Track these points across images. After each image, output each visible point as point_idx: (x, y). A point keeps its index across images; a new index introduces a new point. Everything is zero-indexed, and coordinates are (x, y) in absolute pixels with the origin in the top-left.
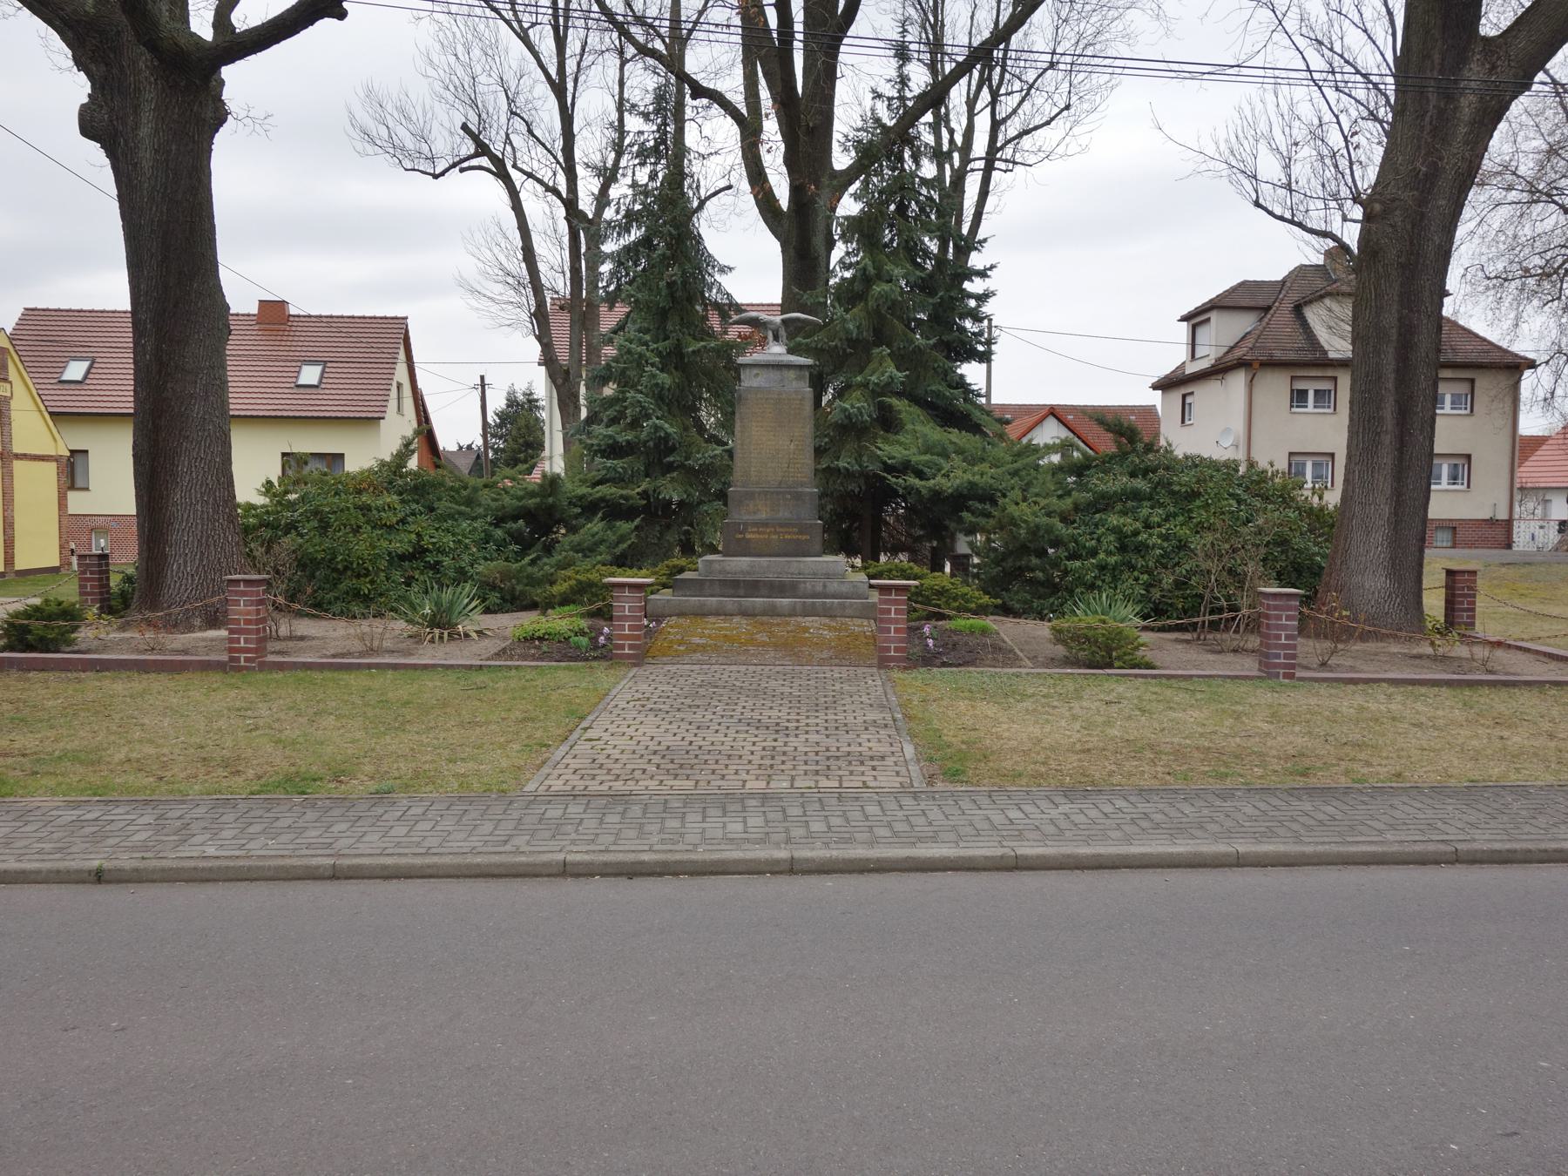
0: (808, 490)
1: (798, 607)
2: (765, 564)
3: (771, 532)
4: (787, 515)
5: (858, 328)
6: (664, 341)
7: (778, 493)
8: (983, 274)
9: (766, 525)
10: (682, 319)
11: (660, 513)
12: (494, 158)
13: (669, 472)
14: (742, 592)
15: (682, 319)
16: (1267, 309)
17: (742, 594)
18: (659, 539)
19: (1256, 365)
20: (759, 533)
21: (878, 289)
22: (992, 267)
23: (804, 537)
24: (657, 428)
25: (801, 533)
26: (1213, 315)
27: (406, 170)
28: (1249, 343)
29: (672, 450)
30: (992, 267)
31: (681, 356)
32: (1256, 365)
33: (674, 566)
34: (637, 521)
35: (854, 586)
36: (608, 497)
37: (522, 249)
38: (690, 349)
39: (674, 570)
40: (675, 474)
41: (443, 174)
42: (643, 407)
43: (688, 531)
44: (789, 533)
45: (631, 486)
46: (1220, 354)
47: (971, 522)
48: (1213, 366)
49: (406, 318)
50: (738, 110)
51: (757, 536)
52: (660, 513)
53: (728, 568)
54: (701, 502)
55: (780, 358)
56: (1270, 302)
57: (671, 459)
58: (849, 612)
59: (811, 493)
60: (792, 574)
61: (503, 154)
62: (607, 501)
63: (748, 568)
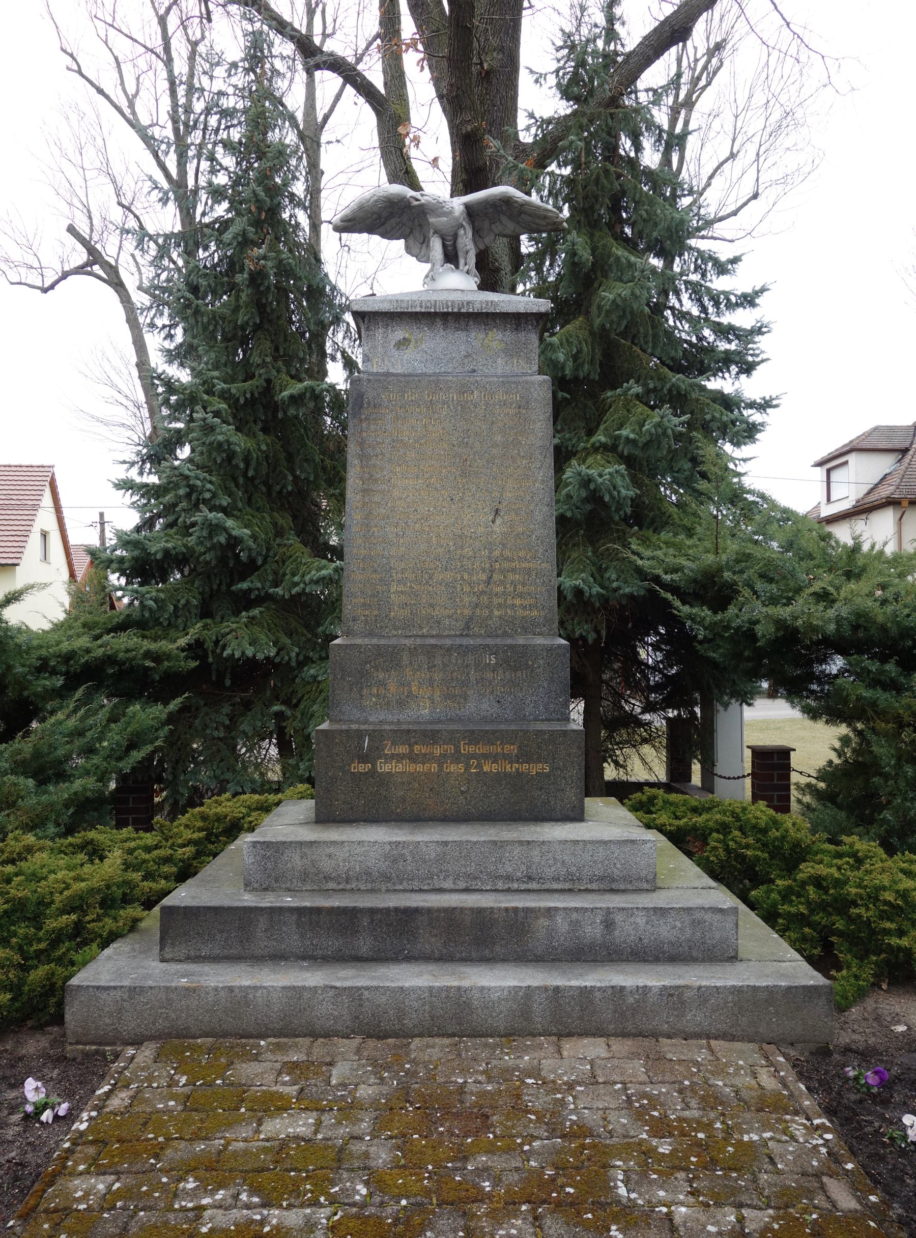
0: (540, 641)
1: (538, 1006)
2: (432, 853)
3: (444, 756)
4: (487, 707)
5: (575, 358)
6: (244, 381)
7: (464, 651)
8: (748, 300)
9: (431, 737)
10: (277, 349)
11: (228, 682)
12: (105, 265)
13: (247, 609)
14: (364, 944)
15: (277, 349)
16: (904, 451)
17: (364, 950)
18: (228, 729)
19: (905, 503)
20: (412, 758)
21: (611, 297)
22: (763, 290)
23: (534, 769)
24: (214, 528)
25: (525, 756)
26: (852, 458)
27: (12, 283)
28: (895, 480)
29: (250, 568)
30: (763, 290)
31: (272, 407)
32: (905, 503)
33: (219, 818)
34: (175, 705)
35: (696, 923)
36: (121, 655)
37: (137, 365)
38: (286, 393)
39: (218, 828)
40: (256, 612)
41: (52, 287)
42: (192, 488)
43: (282, 713)
44: (495, 759)
45: (172, 633)
46: (861, 495)
47: (859, 698)
48: (854, 507)
49: (52, 467)
50: (371, 85)
51: (411, 768)
52: (228, 682)
53: (326, 865)
54: (301, 664)
55: (470, 297)
56: (907, 445)
57: (245, 585)
58: (694, 1018)
59: (550, 649)
60: (509, 878)
61: (117, 261)
62: (121, 663)
63: (384, 866)
